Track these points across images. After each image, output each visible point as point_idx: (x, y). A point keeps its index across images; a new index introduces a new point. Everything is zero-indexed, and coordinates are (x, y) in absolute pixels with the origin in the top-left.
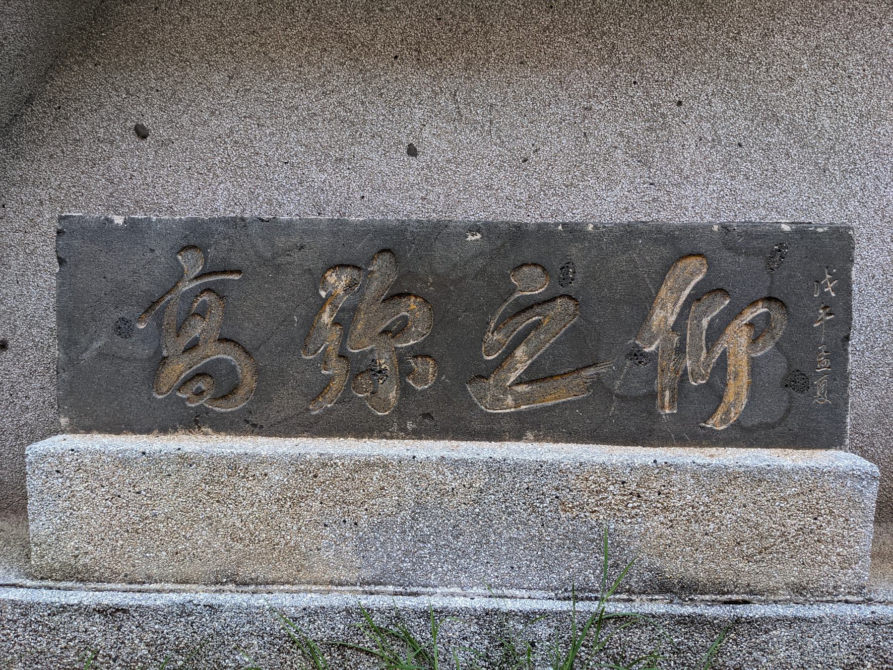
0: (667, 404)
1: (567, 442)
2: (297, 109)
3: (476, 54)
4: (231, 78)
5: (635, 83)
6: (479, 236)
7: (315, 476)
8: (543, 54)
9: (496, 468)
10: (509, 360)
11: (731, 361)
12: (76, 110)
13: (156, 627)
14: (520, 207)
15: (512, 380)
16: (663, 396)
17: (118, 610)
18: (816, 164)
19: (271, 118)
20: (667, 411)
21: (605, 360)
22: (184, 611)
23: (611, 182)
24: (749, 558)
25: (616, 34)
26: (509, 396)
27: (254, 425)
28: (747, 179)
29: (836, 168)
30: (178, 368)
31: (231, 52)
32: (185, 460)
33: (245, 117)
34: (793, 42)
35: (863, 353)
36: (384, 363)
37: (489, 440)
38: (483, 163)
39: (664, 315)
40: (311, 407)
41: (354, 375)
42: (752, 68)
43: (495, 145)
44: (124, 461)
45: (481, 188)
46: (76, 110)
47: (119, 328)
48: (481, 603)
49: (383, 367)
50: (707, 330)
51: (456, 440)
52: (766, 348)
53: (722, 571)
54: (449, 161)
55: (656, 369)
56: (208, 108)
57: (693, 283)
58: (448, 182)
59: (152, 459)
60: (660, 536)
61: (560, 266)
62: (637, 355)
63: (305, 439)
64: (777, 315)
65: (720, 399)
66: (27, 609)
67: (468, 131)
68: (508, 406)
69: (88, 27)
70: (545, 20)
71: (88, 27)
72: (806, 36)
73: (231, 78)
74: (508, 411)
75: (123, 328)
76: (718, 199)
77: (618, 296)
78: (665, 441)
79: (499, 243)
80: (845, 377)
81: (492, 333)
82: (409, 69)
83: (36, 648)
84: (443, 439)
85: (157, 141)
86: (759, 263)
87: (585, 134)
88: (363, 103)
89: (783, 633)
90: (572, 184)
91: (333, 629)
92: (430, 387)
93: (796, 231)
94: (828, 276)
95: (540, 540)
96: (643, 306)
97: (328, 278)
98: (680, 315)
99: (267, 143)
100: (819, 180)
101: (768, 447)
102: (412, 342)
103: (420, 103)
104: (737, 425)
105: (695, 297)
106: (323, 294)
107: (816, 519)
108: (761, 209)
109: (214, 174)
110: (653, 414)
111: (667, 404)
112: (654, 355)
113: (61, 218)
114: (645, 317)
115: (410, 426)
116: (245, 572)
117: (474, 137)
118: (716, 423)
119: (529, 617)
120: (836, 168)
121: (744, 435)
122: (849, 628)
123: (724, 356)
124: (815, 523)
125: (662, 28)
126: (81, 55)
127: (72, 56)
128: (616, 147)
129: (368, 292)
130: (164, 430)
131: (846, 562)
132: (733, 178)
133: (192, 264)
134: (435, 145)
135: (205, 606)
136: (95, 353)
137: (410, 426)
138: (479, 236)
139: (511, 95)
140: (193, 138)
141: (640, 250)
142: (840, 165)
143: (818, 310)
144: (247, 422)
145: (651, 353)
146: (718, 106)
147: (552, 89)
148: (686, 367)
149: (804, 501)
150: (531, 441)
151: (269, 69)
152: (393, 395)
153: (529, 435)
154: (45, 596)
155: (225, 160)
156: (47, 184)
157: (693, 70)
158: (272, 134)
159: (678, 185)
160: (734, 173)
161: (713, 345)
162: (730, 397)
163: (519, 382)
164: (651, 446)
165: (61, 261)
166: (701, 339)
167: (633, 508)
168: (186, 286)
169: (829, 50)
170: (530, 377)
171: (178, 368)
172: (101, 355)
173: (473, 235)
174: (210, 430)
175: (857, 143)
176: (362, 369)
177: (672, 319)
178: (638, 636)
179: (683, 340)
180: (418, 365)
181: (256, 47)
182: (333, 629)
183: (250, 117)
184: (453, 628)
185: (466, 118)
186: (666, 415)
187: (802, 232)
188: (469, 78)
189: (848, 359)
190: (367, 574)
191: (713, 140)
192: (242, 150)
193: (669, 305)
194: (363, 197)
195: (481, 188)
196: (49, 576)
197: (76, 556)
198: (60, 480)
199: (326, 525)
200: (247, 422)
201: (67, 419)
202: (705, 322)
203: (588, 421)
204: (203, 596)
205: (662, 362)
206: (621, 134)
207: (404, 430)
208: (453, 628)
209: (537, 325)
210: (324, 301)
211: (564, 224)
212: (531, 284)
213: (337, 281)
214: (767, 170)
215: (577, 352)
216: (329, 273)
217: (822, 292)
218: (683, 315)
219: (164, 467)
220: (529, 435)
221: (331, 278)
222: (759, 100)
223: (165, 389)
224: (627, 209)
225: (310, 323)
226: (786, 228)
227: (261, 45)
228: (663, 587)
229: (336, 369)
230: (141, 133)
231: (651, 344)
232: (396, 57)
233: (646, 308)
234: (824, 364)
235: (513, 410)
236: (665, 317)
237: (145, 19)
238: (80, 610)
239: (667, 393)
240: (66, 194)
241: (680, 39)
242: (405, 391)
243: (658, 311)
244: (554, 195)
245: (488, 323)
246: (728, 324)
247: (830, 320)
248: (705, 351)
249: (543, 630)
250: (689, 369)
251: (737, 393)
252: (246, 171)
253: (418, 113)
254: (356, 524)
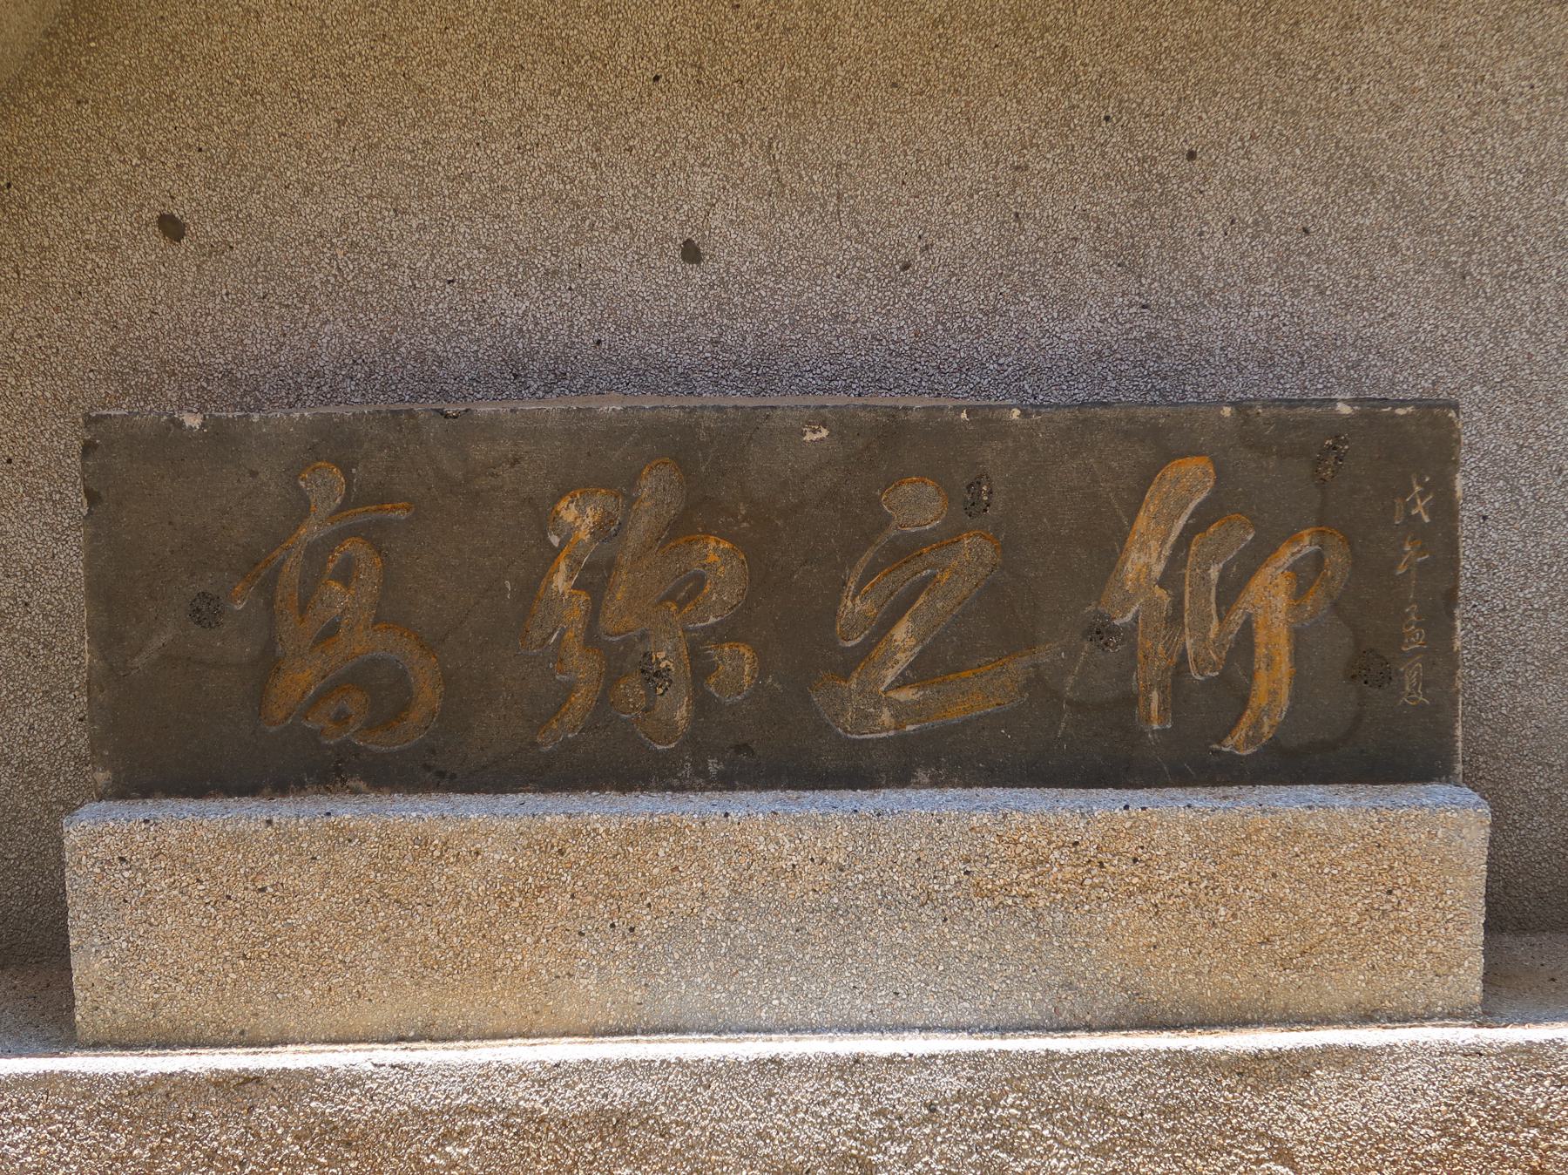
0: (1154, 714)
1: (988, 785)
2: (469, 179)
3: (807, 71)
4: (341, 123)
5: (1107, 119)
6: (824, 433)
7: (561, 852)
8: (932, 68)
10: (883, 645)
11: (1261, 637)
12: (41, 190)
13: (313, 1104)
14: (899, 355)
15: (888, 681)
16: (1148, 700)
17: (247, 1080)
18: (1448, 264)
19: (420, 198)
20: (1156, 726)
21: (1047, 641)
24: (1284, 964)
25: (1069, 30)
26: (885, 709)
27: (441, 774)
28: (1322, 293)
29: (1485, 270)
31: (342, 75)
33: (370, 197)
34: (1397, 38)
35: (1545, 612)
37: (853, 787)
38: (826, 272)
39: (1143, 559)
40: (539, 740)
42: (1323, 88)
43: (848, 238)
45: (823, 320)
46: (41, 190)
47: (199, 610)
49: (663, 665)
50: (1218, 586)
51: (794, 788)
54: (761, 271)
55: (1133, 655)
56: (298, 181)
57: (1192, 506)
58: (761, 310)
60: (1138, 932)
61: (967, 481)
62: (1101, 632)
63: (531, 795)
65: (1244, 702)
67: (795, 214)
69: (61, 30)
71: (61, 30)
72: (1422, 29)
73: (341, 123)
74: (884, 735)
75: (205, 611)
76: (1269, 333)
77: (1065, 532)
79: (860, 443)
80: (1452, 659)
81: (853, 600)
82: (682, 101)
83: (107, 1152)
84: (773, 788)
85: (202, 246)
87: (1017, 215)
88: (595, 166)
90: (995, 310)
91: (605, 1096)
92: (746, 698)
93: (1361, 415)
94: (1417, 489)
95: (941, 946)
96: (1107, 545)
97: (563, 513)
98: (1172, 560)
99: (414, 245)
100: (1454, 294)
101: (1327, 783)
102: (712, 620)
103: (703, 164)
104: (1274, 746)
106: (555, 540)
107: (1390, 892)
108: (1349, 349)
109: (312, 305)
111: (1154, 714)
112: (1132, 628)
113: (90, 421)
115: (713, 767)
118: (1237, 743)
120: (1485, 270)
123: (1248, 628)
124: (1389, 901)
125: (1154, 18)
126: (49, 84)
127: (32, 86)
128: (1076, 239)
129: (632, 535)
132: (1295, 293)
133: (326, 487)
135: (393, 1067)
136: (155, 656)
137: (713, 767)
138: (824, 433)
139: (875, 146)
140: (270, 238)
141: (1101, 451)
142: (1492, 265)
143: (1402, 546)
144: (427, 768)
145: (1125, 627)
146: (1263, 158)
147: (953, 133)
148: (1185, 650)
149: (1370, 864)
150: (925, 787)
151: (415, 104)
152: (681, 714)
153: (922, 776)
155: (332, 280)
157: (1215, 93)
158: (423, 228)
159: (1193, 308)
160: (1297, 284)
161: (1228, 611)
162: (1259, 698)
163: (902, 682)
164: (1129, 786)
165: (92, 497)
166: (1208, 600)
167: (1093, 887)
168: (310, 531)
169: (1465, 51)
170: (917, 674)
173: (814, 431)
174: (362, 785)
175: (1522, 223)
177: (1158, 569)
179: (1178, 604)
181: (388, 64)
182: (605, 1096)
183: (380, 196)
185: (792, 190)
186: (1153, 732)
187: (1372, 411)
188: (794, 116)
189: (1454, 628)
191: (1256, 223)
192: (364, 260)
193: (1153, 543)
194: (599, 342)
195: (823, 320)
197: (154, 1006)
198: (126, 874)
199: (581, 934)
200: (427, 768)
201: (108, 774)
202: (1214, 573)
203: (1022, 748)
205: (1144, 643)
206: (1084, 215)
207: (702, 773)
209: (923, 584)
210: (556, 552)
211: (971, 411)
214: (1357, 277)
216: (563, 504)
217: (1409, 516)
218: (1176, 561)
219: (305, 845)
220: (922, 776)
222: (1337, 146)
223: (280, 715)
224: (1099, 353)
225: (532, 588)
226: (1344, 409)
227: (399, 61)
231: (1125, 612)
232: (656, 78)
233: (1114, 550)
234: (1415, 639)
235: (892, 733)
236: (1148, 565)
237: (175, 14)
239: (1155, 695)
240: (25, 351)
241: (1187, 37)
242: (703, 704)
243: (1134, 555)
244: (961, 330)
245: (845, 584)
246: (1251, 573)
247: (1422, 563)
248: (1215, 621)
250: (1190, 653)
252: (373, 299)
253: (701, 183)
254: (632, 930)
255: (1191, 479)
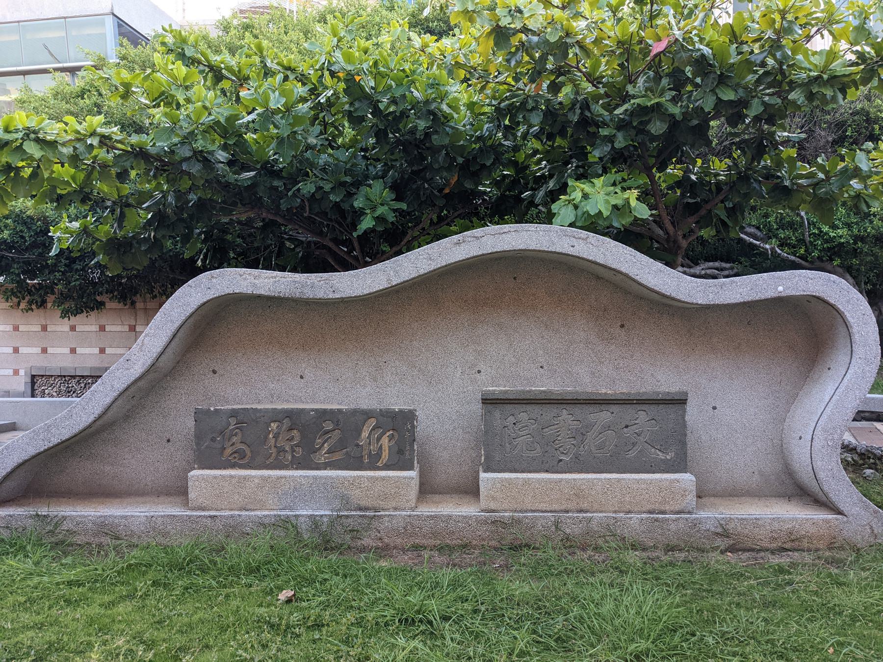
9: (315, 478)
22: (232, 516)
23: (365, 387)
30: (229, 451)
32: (232, 477)
36: (287, 449)
39: (365, 434)
41: (279, 452)
44: (215, 477)
48: (310, 512)
52: (393, 443)
53: (375, 504)
59: (223, 477)
62: (358, 445)
64: (395, 434)
66: (190, 517)
68: (322, 460)
70: (343, 337)
75: (213, 440)
78: (366, 469)
86: (390, 420)
89: (386, 519)
105: (373, 429)
110: (362, 462)
114: (360, 435)
116: (248, 507)
117: (321, 373)
118: (379, 464)
119: (322, 516)
121: (387, 467)
122: (403, 517)
130: (225, 469)
131: (407, 501)
133: (233, 421)
134: (308, 374)
146: (397, 363)
154: (195, 513)
156: (184, 388)
168: (231, 428)
170: (328, 452)
171: (229, 451)
172: (207, 447)
176: (281, 450)
178: (349, 520)
180: (297, 449)
184: (302, 520)
187: (401, 411)
190: (281, 507)
196: (193, 509)
204: (237, 513)
208: (302, 520)
212: (328, 426)
213: (274, 426)
215: (341, 445)
221: (272, 424)
225: (266, 438)
228: (360, 509)
229: (273, 450)
230: (214, 372)
234: (408, 448)
238: (204, 516)
242: (293, 456)
249: (325, 520)
251: (385, 455)
255: (372, 422)
